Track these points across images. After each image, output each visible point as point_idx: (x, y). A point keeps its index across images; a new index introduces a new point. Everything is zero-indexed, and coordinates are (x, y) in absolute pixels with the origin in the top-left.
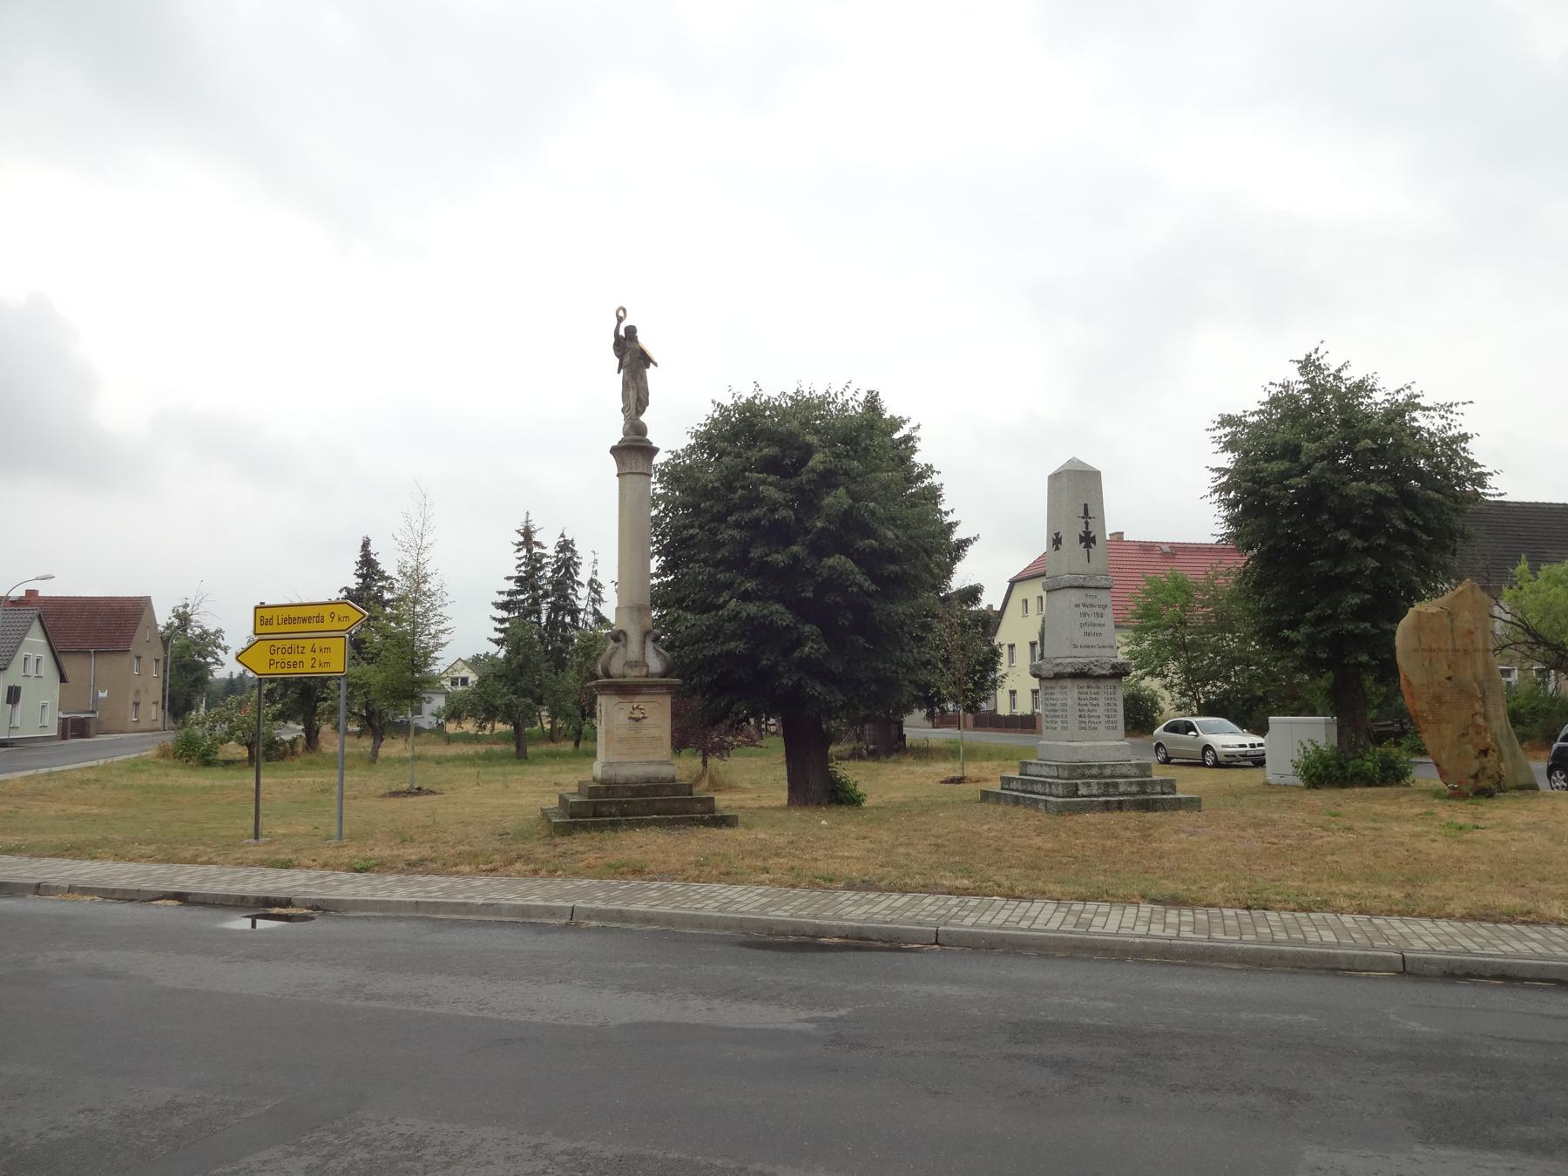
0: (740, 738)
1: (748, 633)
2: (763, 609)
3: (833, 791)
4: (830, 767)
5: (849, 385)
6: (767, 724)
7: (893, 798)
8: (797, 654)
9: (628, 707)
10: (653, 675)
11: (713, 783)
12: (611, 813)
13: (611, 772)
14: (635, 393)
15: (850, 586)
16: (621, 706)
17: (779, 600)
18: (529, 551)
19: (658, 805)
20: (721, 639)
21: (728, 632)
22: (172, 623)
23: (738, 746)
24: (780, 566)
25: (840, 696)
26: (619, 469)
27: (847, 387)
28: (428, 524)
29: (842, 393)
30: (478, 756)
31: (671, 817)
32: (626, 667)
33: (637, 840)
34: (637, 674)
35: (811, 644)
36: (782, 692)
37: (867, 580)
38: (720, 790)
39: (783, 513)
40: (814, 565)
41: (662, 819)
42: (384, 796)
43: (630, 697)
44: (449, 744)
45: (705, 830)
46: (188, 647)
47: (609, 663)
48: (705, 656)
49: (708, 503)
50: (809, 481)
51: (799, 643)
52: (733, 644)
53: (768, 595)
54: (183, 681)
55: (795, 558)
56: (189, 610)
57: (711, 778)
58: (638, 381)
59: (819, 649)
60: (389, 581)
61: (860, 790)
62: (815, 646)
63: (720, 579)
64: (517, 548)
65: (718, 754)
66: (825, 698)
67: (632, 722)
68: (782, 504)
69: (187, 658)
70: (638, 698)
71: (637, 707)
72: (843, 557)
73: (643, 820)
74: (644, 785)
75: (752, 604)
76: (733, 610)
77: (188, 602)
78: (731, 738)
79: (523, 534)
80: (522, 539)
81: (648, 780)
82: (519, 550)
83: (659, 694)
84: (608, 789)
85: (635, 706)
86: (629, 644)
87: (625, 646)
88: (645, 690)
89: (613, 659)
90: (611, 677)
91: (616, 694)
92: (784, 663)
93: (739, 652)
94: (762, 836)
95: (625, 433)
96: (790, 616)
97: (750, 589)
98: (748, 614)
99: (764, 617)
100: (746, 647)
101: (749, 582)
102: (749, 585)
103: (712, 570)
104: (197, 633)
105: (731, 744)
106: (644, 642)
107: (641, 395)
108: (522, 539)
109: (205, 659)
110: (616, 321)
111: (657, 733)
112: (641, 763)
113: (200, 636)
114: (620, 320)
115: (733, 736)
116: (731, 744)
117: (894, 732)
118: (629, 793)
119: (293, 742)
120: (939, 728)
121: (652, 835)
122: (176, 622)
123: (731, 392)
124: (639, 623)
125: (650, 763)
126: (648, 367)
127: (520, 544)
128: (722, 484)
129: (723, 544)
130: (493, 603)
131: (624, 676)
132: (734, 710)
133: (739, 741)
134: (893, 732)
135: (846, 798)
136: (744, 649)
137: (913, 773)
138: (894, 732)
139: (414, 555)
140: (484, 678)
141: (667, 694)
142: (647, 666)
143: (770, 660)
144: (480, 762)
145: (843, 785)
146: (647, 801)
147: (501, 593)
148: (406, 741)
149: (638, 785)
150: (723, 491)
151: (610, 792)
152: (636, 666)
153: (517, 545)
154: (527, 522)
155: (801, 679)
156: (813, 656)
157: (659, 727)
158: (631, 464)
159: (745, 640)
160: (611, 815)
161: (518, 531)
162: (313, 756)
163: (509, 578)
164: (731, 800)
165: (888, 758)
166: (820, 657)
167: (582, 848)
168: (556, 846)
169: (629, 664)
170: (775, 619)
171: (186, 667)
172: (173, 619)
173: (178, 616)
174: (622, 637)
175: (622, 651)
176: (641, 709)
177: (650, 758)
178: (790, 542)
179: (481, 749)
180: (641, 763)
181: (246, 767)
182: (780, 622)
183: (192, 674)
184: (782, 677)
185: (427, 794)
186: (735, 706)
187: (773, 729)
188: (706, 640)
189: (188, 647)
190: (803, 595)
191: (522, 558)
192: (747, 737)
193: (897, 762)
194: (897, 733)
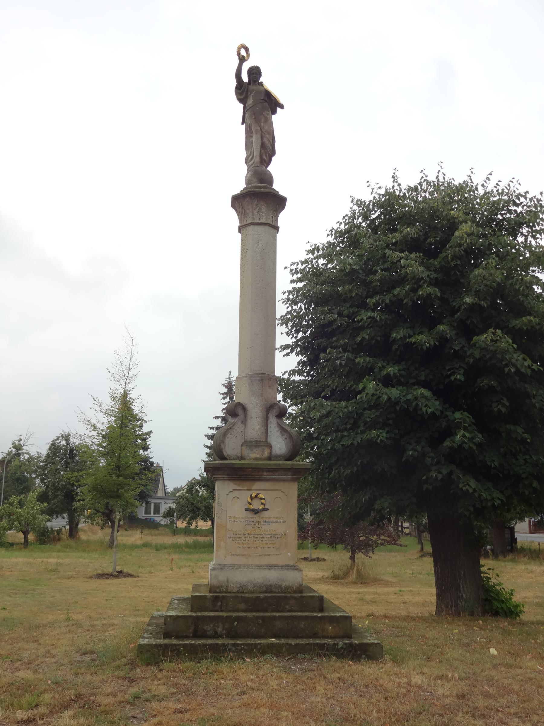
0: (383, 537)
1: (391, 422)
2: (407, 394)
3: (486, 600)
4: (482, 573)
5: (489, 176)
6: (402, 527)
7: (525, 597)
8: (447, 443)
9: (245, 496)
10: (277, 457)
11: (360, 576)
12: (216, 633)
13: (222, 577)
14: (259, 136)
15: (507, 365)
16: (236, 494)
17: (425, 385)
18: (231, 398)
19: (278, 624)
20: (362, 428)
21: (368, 420)
22: (11, 451)
23: (381, 544)
24: (425, 348)
25: (497, 494)
26: (241, 221)
27: (488, 179)
28: (133, 359)
29: (483, 185)
30: (187, 546)
31: (293, 642)
32: (244, 447)
33: (243, 678)
34: (258, 456)
35: (462, 432)
36: (431, 487)
37: (526, 360)
38: (365, 583)
39: (426, 290)
40: (463, 346)
41: (281, 646)
42: (91, 577)
43: (247, 483)
44: (174, 535)
45: (338, 664)
46: (20, 466)
47: (223, 442)
48: (343, 445)
49: (347, 287)
50: (454, 257)
51: (449, 432)
52: (374, 433)
53: (412, 381)
54: (16, 489)
55: (444, 340)
56: (22, 443)
57: (358, 572)
58: (262, 124)
59: (473, 438)
60: (140, 422)
61: (516, 598)
62: (467, 435)
63: (359, 363)
64: (223, 396)
65: (363, 551)
66: (480, 496)
67: (250, 515)
68: (425, 282)
69: (19, 474)
70: (258, 485)
71: (256, 496)
72: (499, 332)
73: (256, 645)
74: (262, 595)
75: (395, 389)
76: (373, 395)
77: (21, 437)
78: (375, 537)
79: (227, 387)
80: (226, 390)
81: (269, 589)
82: (224, 398)
83: (283, 480)
84: (216, 599)
85: (254, 495)
86: (249, 421)
87: (244, 422)
88: (266, 475)
89: (229, 436)
90: (226, 459)
91: (230, 480)
92: (432, 455)
93: (381, 440)
94: (417, 679)
95: (248, 182)
96: (437, 403)
97: (392, 373)
98: (389, 399)
99: (408, 402)
100: (389, 435)
101: (391, 367)
102: (391, 370)
103: (351, 356)
104: (26, 458)
105: (375, 542)
106: (267, 418)
107: (265, 140)
108: (226, 390)
109: (30, 475)
110: (237, 62)
111: (280, 529)
112: (260, 567)
113: (28, 460)
114: (242, 60)
115: (377, 536)
116: (375, 542)
117: (508, 536)
118: (243, 606)
119: (59, 532)
120: (535, 533)
121: (266, 669)
122: (14, 451)
123: (370, 188)
124: (262, 395)
125: (271, 567)
126: (274, 112)
127: (225, 394)
128: (361, 268)
129: (362, 328)
130: (205, 435)
131: (242, 458)
132: (376, 507)
133: (382, 540)
134: (507, 536)
135: (502, 608)
136: (387, 438)
137: (532, 572)
138: (508, 536)
139: (123, 384)
140: (191, 487)
141: (293, 480)
142: (270, 447)
143: (416, 451)
144: (186, 550)
145: (498, 593)
146: (263, 618)
147: (211, 428)
148: (142, 532)
149: (255, 595)
150: (362, 275)
151: (219, 604)
152: (256, 446)
153: (223, 394)
154: (230, 378)
155: (451, 472)
156: (466, 447)
157: (283, 522)
158: (253, 215)
159: (387, 429)
160: (216, 636)
161: (224, 385)
162: (72, 542)
163: (217, 418)
164: (375, 593)
165: (505, 557)
166: (475, 448)
167: (162, 690)
168: (132, 681)
169: (249, 444)
170: (420, 404)
171: (18, 479)
172: (12, 449)
173: (15, 447)
174: (240, 411)
175: (239, 427)
176: (261, 499)
177: (273, 560)
178: (431, 324)
179: (190, 540)
180: (260, 567)
181: (21, 549)
182: (424, 409)
183: (22, 484)
184: (430, 470)
185: (125, 577)
186: (379, 502)
187: (407, 531)
188: (346, 429)
189: (20, 466)
190: (453, 378)
191: (226, 403)
192: (389, 537)
193: (513, 560)
194: (510, 536)
